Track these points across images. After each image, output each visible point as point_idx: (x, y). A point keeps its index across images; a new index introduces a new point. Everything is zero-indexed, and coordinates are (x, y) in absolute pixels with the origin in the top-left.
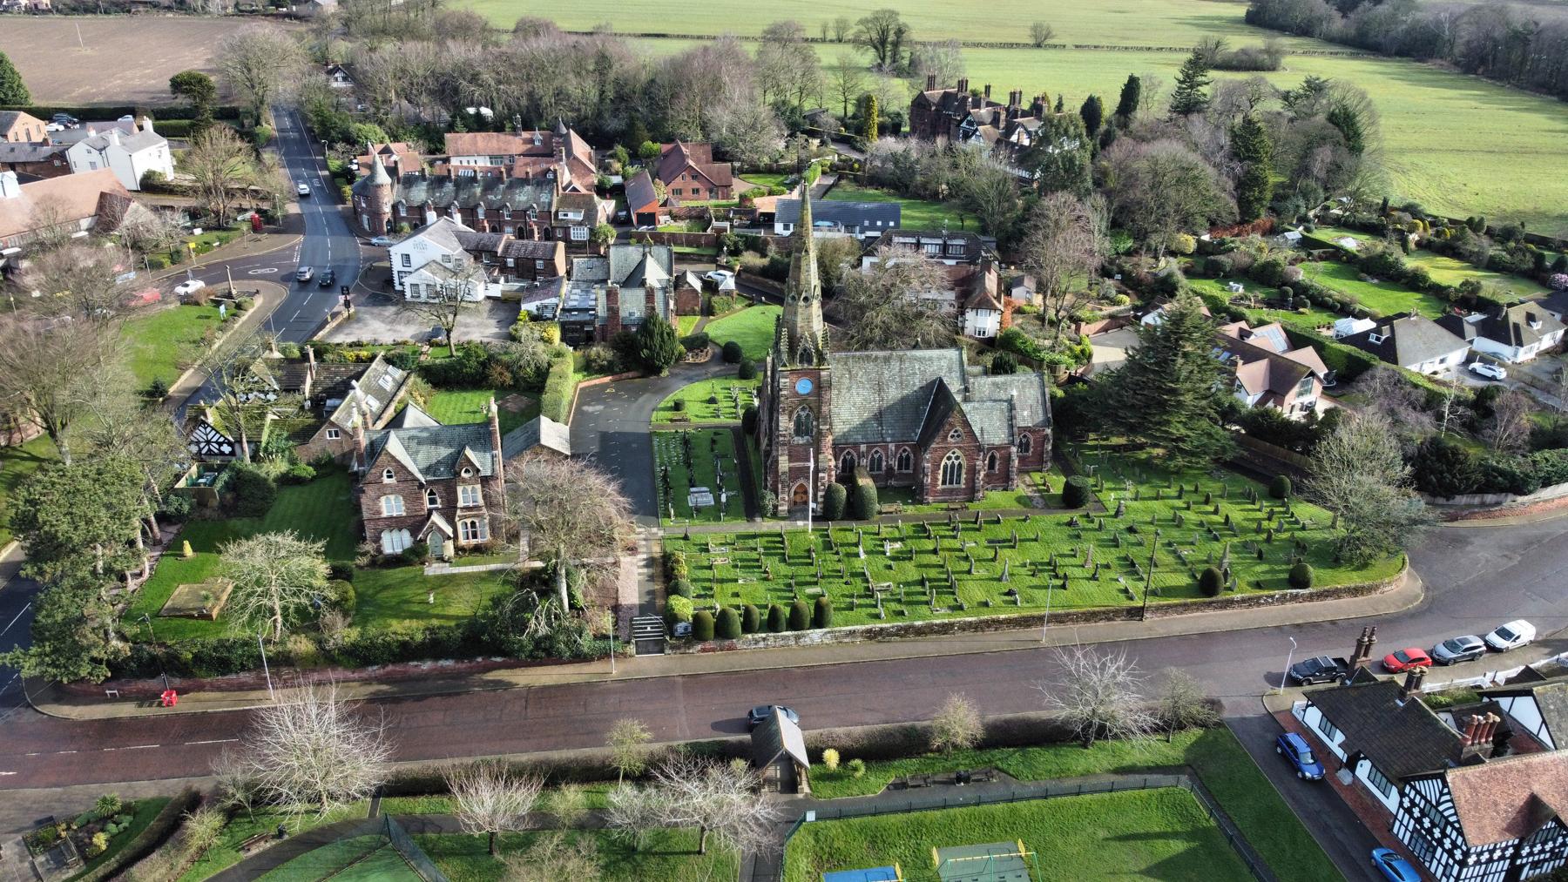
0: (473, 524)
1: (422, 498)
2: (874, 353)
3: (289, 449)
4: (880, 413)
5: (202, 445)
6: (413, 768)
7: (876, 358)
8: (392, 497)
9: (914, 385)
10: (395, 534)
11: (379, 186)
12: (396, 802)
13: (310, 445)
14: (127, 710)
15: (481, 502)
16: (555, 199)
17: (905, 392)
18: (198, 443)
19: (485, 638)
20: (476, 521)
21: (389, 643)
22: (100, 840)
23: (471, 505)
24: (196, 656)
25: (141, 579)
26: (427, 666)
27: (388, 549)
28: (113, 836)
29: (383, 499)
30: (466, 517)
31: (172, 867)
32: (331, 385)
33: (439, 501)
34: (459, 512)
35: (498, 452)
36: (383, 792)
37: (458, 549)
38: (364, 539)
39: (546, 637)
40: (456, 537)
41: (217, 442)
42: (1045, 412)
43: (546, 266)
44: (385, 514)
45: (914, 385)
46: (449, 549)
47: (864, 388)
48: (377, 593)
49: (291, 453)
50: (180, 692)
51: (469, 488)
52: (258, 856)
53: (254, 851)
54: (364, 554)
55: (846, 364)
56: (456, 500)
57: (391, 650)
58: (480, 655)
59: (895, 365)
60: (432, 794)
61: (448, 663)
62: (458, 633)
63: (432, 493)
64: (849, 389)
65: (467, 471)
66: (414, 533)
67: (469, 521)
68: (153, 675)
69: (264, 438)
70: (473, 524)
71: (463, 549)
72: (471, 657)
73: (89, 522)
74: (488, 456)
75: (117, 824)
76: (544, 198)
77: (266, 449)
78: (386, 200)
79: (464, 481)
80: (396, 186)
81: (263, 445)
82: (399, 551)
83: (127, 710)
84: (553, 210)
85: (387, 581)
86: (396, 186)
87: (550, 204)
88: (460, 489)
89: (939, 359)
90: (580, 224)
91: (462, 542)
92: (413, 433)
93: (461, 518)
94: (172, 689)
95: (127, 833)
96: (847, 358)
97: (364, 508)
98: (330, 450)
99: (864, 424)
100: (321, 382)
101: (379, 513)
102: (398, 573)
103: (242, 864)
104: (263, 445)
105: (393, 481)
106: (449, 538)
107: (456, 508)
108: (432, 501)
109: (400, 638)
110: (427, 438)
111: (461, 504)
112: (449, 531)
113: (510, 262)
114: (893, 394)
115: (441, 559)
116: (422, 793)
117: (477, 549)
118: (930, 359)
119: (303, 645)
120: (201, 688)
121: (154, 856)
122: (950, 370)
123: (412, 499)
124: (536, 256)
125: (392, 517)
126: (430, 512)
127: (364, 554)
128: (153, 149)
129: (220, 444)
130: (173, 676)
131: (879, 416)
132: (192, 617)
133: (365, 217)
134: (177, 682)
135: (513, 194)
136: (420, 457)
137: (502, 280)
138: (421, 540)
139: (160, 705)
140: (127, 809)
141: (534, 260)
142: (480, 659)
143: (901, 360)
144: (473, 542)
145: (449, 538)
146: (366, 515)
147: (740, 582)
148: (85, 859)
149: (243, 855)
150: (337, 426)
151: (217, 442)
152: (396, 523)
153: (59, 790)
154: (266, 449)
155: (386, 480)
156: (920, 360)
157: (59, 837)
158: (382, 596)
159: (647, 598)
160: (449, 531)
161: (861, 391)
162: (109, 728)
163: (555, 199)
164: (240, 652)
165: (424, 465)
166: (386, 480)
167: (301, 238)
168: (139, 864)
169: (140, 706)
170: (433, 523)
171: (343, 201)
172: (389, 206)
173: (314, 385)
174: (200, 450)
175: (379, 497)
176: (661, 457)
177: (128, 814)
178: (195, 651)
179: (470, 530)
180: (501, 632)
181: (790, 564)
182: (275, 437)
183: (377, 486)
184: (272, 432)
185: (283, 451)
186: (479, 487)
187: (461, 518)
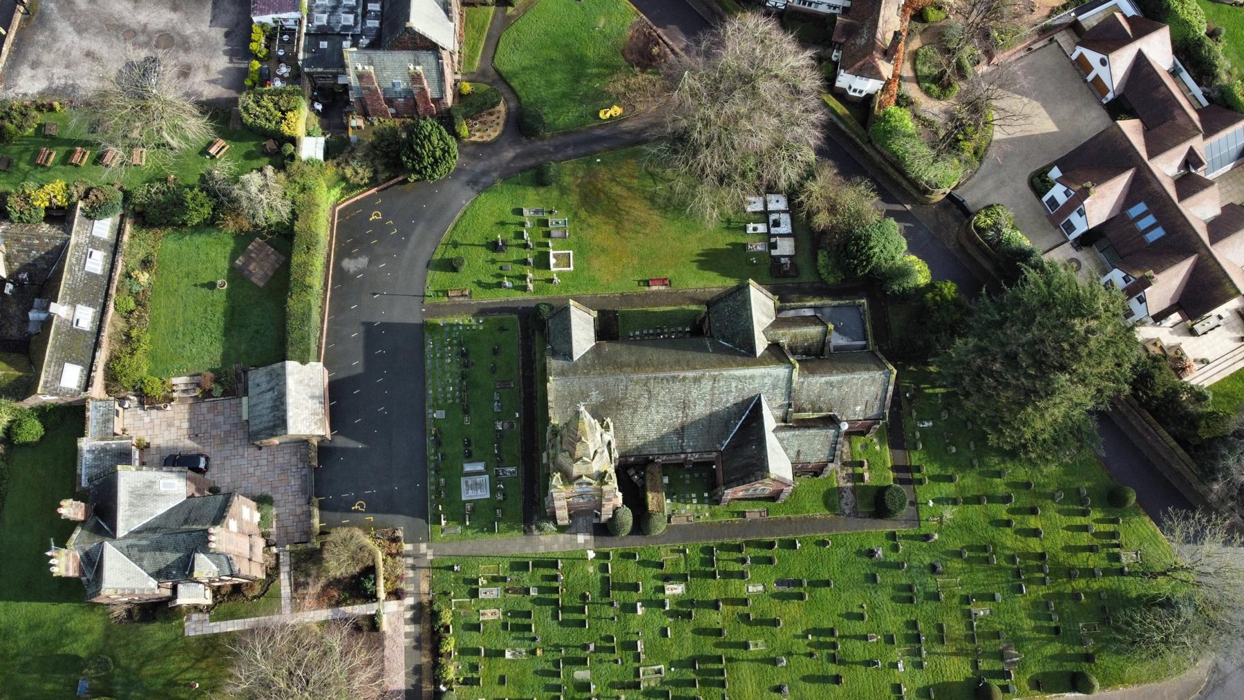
2: (682, 374)
4: (683, 428)
7: (684, 378)
9: (728, 401)
17: (715, 409)
32: (30, 261)
42: (883, 406)
45: (728, 401)
47: (665, 407)
48: (142, 665)
55: (645, 385)
59: (707, 385)
64: (647, 408)
85: (151, 646)
89: (763, 377)
92: (130, 541)
96: (648, 379)
99: (662, 439)
100: (16, 257)
110: (148, 546)
114: (700, 410)
118: (752, 377)
122: (774, 387)
131: (681, 431)
136: (145, 563)
143: (715, 379)
147: (508, 655)
156: (739, 379)
158: (148, 670)
159: (413, 681)
161: (661, 409)
176: (435, 391)
181: (564, 624)
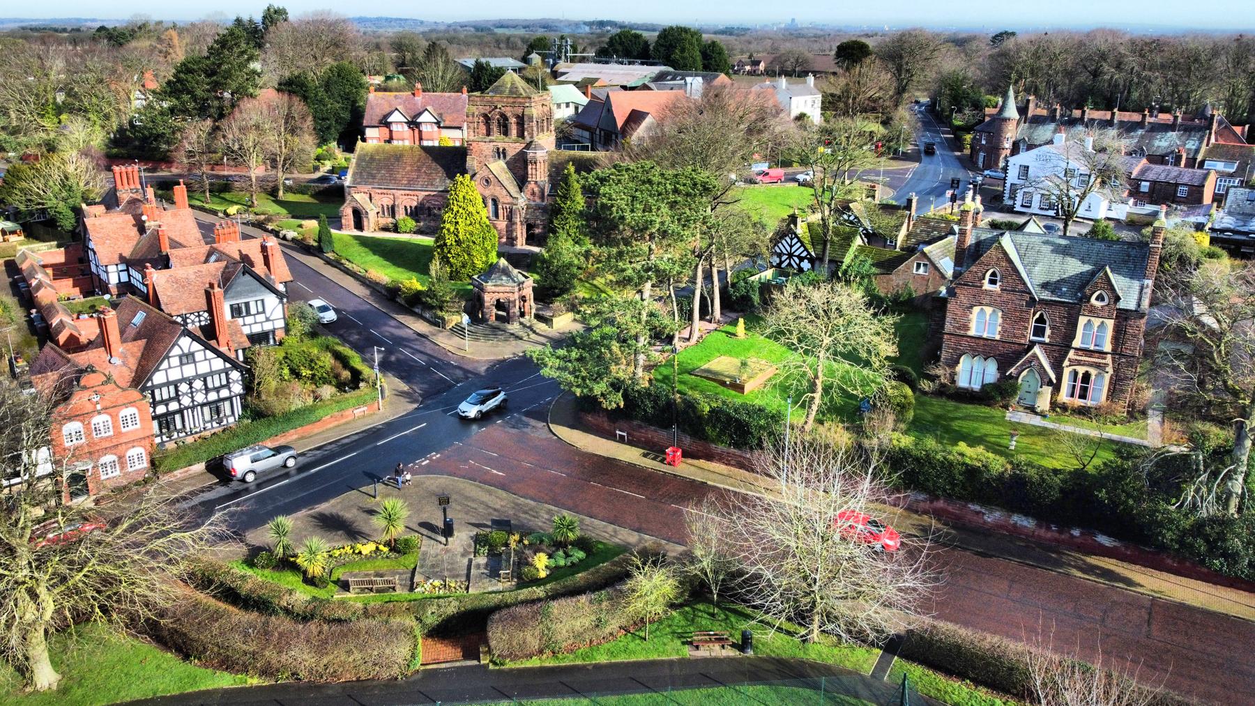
0: (1086, 377)
1: (1027, 320)
3: (869, 276)
5: (784, 258)
6: (952, 630)
8: (989, 310)
10: (977, 363)
11: (1006, 120)
12: (917, 672)
13: (893, 277)
14: (630, 455)
15: (1108, 347)
16: (1204, 148)
18: (780, 255)
19: (1103, 494)
20: (1093, 372)
21: (951, 464)
22: (541, 562)
23: (1092, 348)
24: (712, 411)
25: (688, 343)
26: (993, 517)
27: (962, 382)
28: (557, 567)
29: (976, 309)
30: (1079, 363)
31: (599, 624)
33: (1048, 332)
34: (1071, 354)
35: (1149, 283)
36: (896, 646)
37: (1054, 405)
38: (937, 359)
39: (1213, 520)
40: (1057, 388)
41: (798, 256)
43: (1190, 193)
44: (972, 332)
46: (1043, 403)
49: (870, 282)
50: (686, 455)
51: (1096, 322)
52: (706, 661)
53: (703, 653)
54: (933, 378)
56: (1073, 338)
57: (951, 478)
58: (1078, 526)
60: (977, 682)
61: (1027, 523)
62: (1057, 480)
63: (1041, 320)
65: (1100, 298)
66: (1002, 368)
67: (1081, 370)
68: (666, 425)
69: (847, 260)
70: (1086, 377)
71: (1064, 408)
72: (1065, 525)
73: (647, 209)
74: (1136, 284)
75: (567, 555)
76: (1191, 145)
77: (845, 273)
78: (1009, 135)
79: (1093, 312)
80: (1022, 124)
81: (844, 267)
82: (976, 386)
83: (630, 455)
84: (1200, 158)
86: (1022, 124)
87: (1197, 151)
88: (1082, 320)
90: (1231, 175)
91: (1063, 397)
93: (1072, 362)
94: (679, 447)
95: (574, 568)
97: (949, 318)
98: (912, 286)
101: (967, 328)
102: (970, 409)
103: (683, 662)
104: (844, 267)
105: (997, 288)
106: (1050, 383)
107: (1069, 347)
108: (1039, 332)
109: (968, 461)
111: (1077, 343)
112: (1053, 377)
113: (1145, 187)
115: (1032, 410)
116: (962, 676)
117: (1083, 412)
119: (838, 436)
120: (709, 457)
121: (583, 599)
123: (1013, 318)
124: (1180, 181)
125: (980, 338)
126: (1033, 344)
127: (933, 378)
128: (809, 98)
129: (801, 259)
130: (684, 431)
132: (723, 383)
133: (982, 154)
134: (687, 440)
135: (1152, 138)
137: (1131, 201)
138: (1011, 376)
139: (662, 461)
140: (582, 543)
141: (1177, 185)
142: (1076, 533)
144: (1079, 402)
145: (1050, 383)
146: (948, 327)
148: (519, 577)
149: (688, 652)
150: (929, 259)
151: (798, 256)
152: (983, 348)
153: (532, 503)
154: (845, 273)
155: (987, 286)
157: (507, 545)
160: (1053, 377)
162: (606, 466)
163: (1204, 148)
164: (762, 422)
165: (1043, 279)
166: (987, 286)
167: (917, 165)
168: (563, 601)
169: (645, 455)
170: (1035, 356)
171: (961, 149)
172: (1011, 141)
173: (908, 236)
174: (781, 262)
175: (971, 307)
177: (581, 549)
178: (714, 405)
179: (1079, 384)
180: (1129, 496)
182: (858, 262)
183: (975, 290)
184: (856, 257)
185: (862, 278)
186: (1110, 324)
187: (1073, 363)
